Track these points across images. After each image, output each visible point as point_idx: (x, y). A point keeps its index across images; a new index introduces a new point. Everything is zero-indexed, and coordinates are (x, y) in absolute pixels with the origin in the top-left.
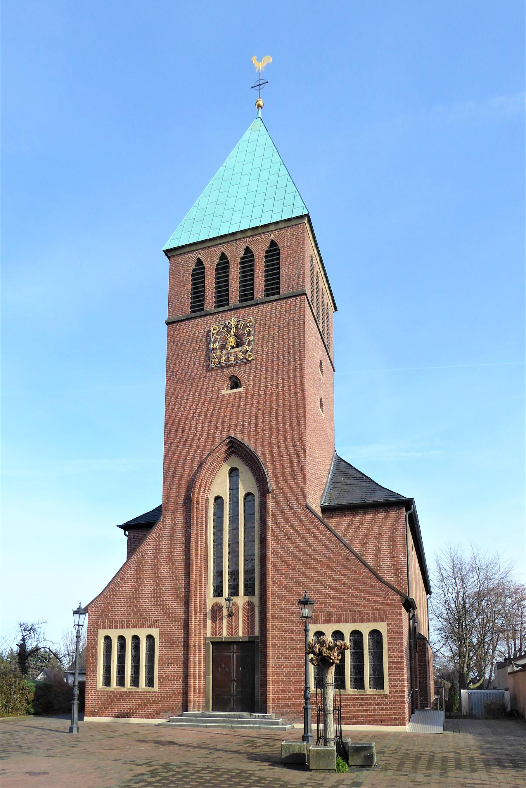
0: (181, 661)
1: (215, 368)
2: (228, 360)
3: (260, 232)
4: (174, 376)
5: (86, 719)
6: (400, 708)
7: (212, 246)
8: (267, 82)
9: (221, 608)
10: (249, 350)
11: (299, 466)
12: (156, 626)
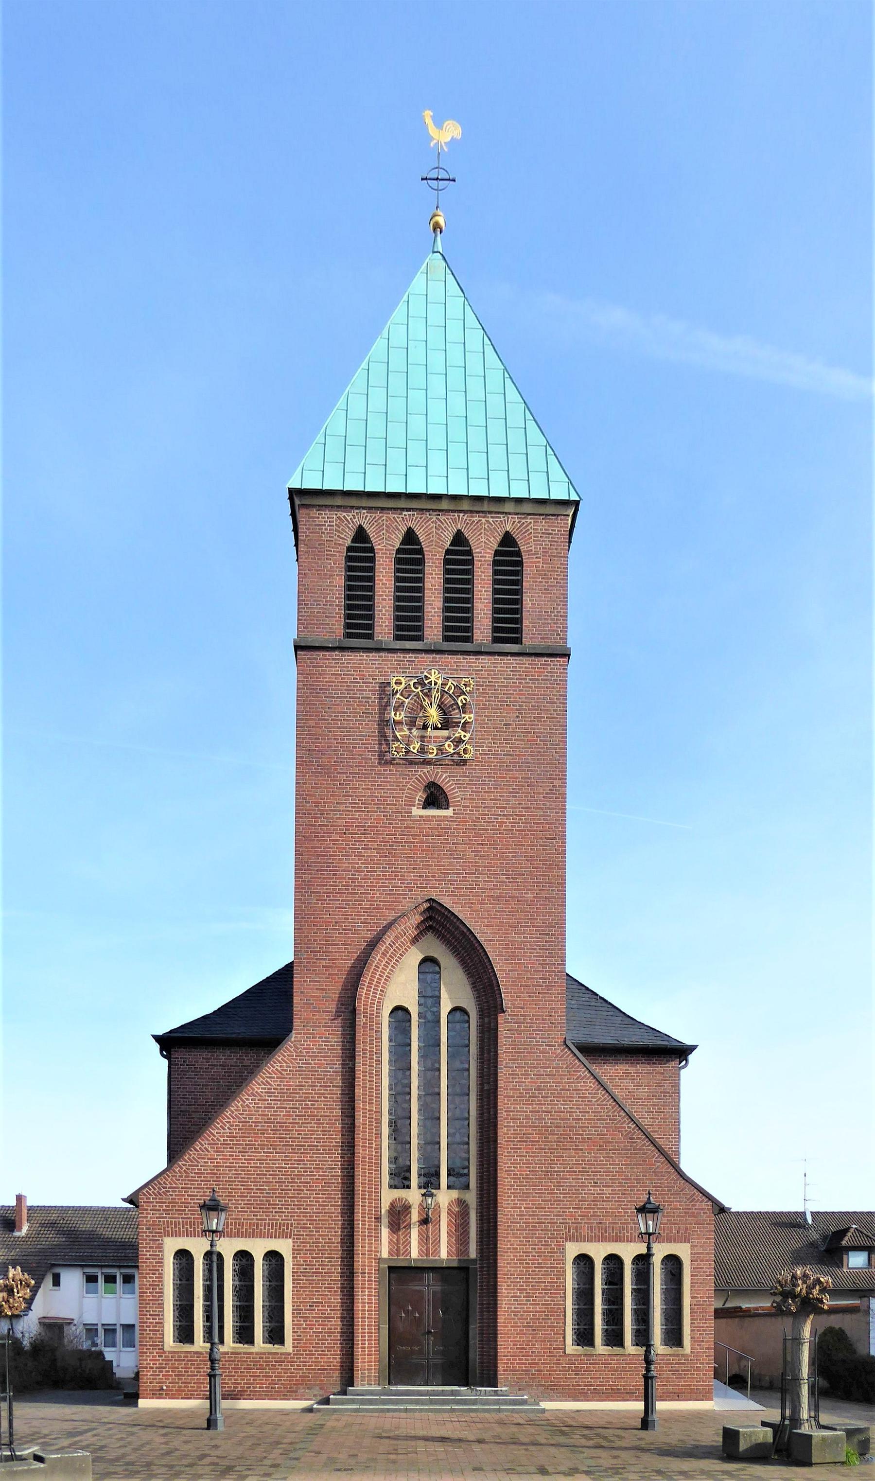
0: (336, 1300)
1: (397, 761)
2: (422, 750)
3: (485, 507)
4: (313, 762)
5: (142, 1403)
7: (389, 509)
8: (454, 181)
9: (407, 1208)
10: (466, 739)
11: (554, 971)
12: (285, 1235)
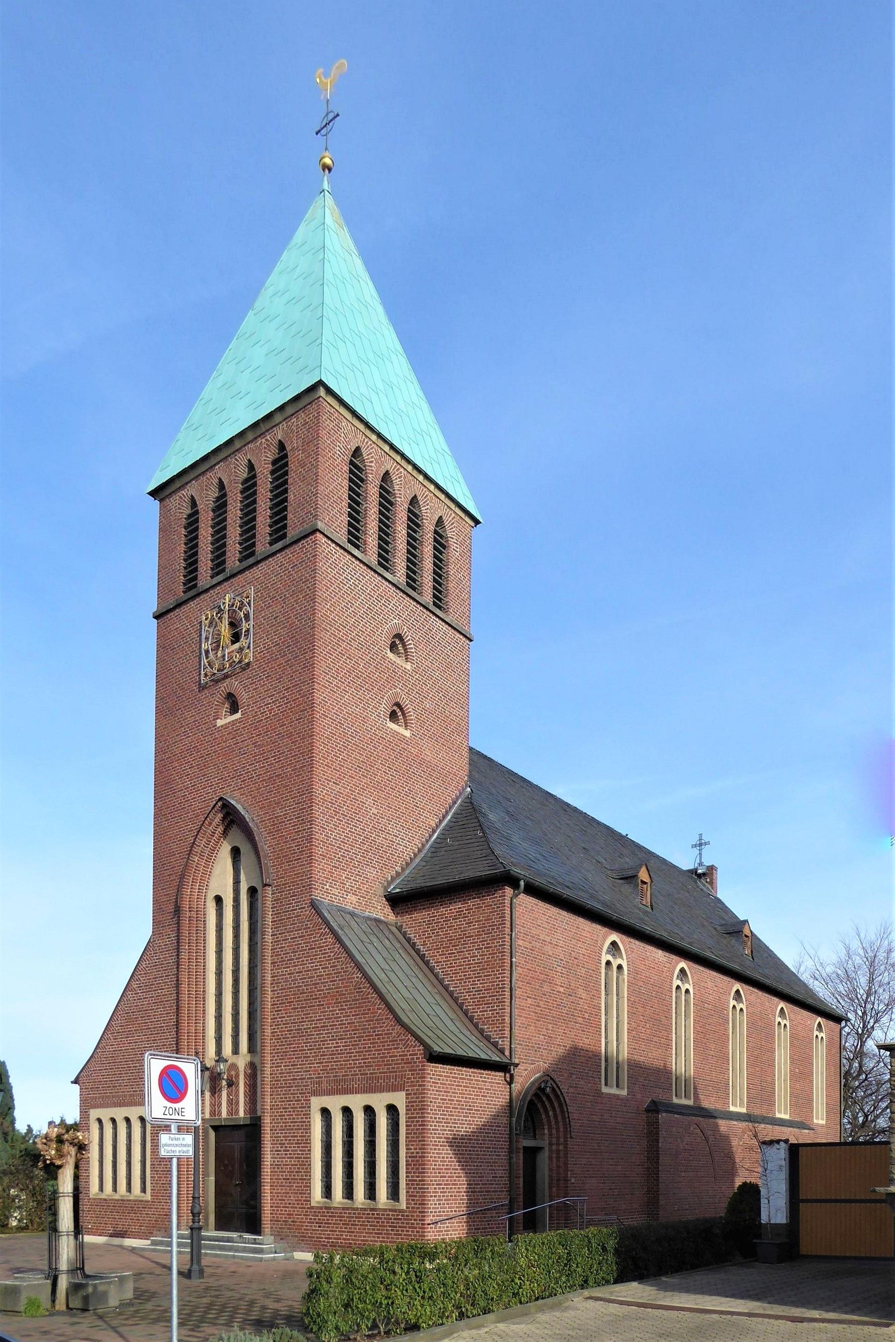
6: (418, 1232)
7: (207, 470)
8: (338, 115)
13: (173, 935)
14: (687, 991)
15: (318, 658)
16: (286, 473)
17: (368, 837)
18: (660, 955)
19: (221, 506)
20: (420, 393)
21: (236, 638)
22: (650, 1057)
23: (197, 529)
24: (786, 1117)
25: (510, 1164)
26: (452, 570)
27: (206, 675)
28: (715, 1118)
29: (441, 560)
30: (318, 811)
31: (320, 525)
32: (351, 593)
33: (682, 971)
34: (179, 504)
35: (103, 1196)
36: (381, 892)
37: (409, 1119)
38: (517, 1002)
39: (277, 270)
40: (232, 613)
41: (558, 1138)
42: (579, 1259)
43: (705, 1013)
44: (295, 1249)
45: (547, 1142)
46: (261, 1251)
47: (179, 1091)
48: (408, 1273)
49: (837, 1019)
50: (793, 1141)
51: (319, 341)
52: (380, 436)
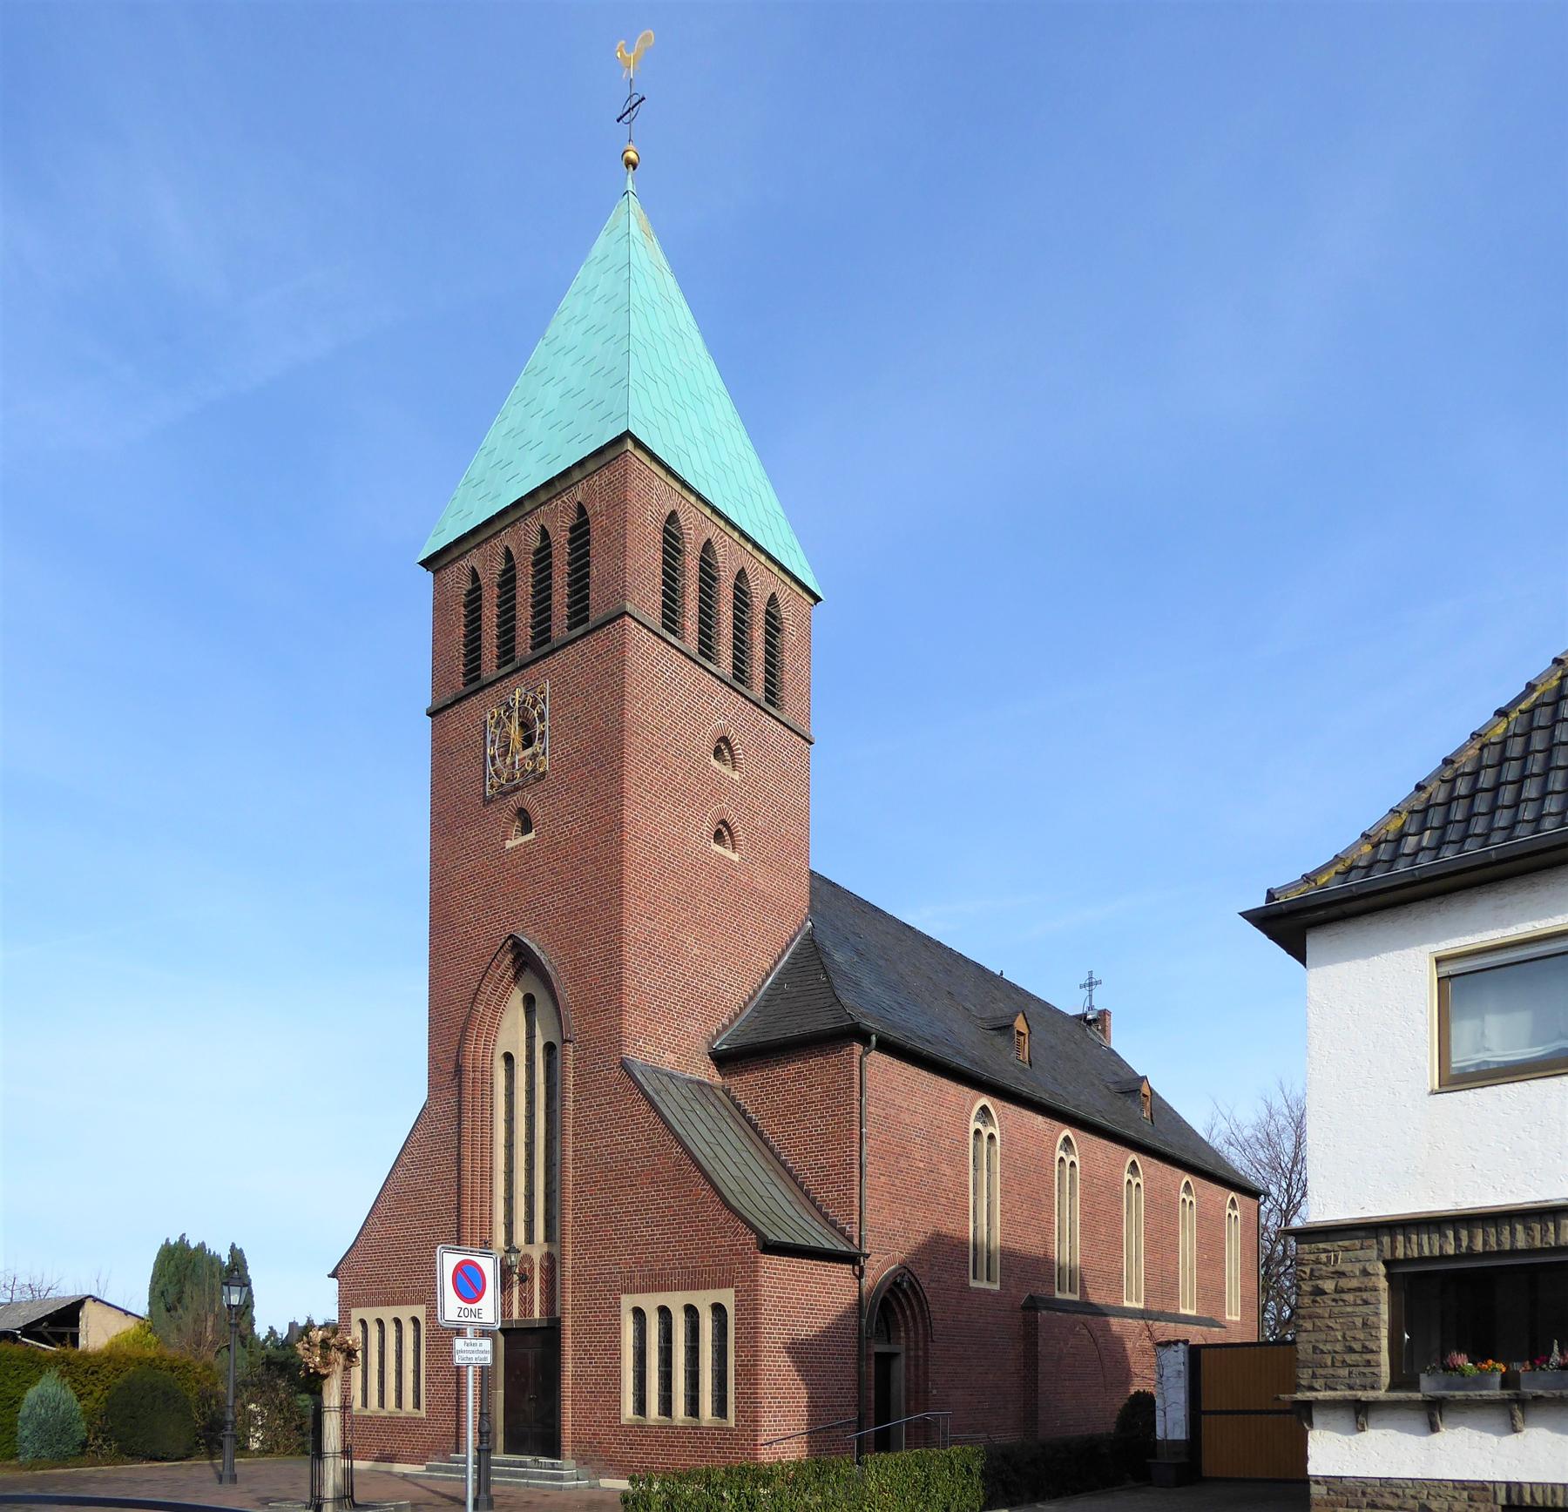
13: (453, 1100)
14: (1073, 1164)
15: (628, 767)
16: (588, 543)
17: (690, 981)
18: (1039, 1121)
19: (508, 581)
20: (748, 442)
21: (528, 742)
22: (1028, 1244)
23: (480, 607)
24: (1193, 1313)
25: (859, 1373)
26: (787, 658)
27: (492, 786)
28: (1106, 1315)
29: (774, 647)
30: (629, 952)
31: (629, 607)
32: (668, 690)
33: (1067, 1139)
34: (450, 574)
35: (367, 1413)
36: (704, 1049)
37: (738, 1321)
38: (867, 1180)
39: (573, 289)
40: (524, 712)
41: (916, 1343)
42: (939, 1484)
43: (1094, 1190)
44: (600, 1474)
45: (903, 1347)
46: (560, 1478)
47: (474, 1287)
48: (738, 1499)
49: (1254, 1193)
50: (1196, 1340)
51: (625, 383)
52: (699, 497)
